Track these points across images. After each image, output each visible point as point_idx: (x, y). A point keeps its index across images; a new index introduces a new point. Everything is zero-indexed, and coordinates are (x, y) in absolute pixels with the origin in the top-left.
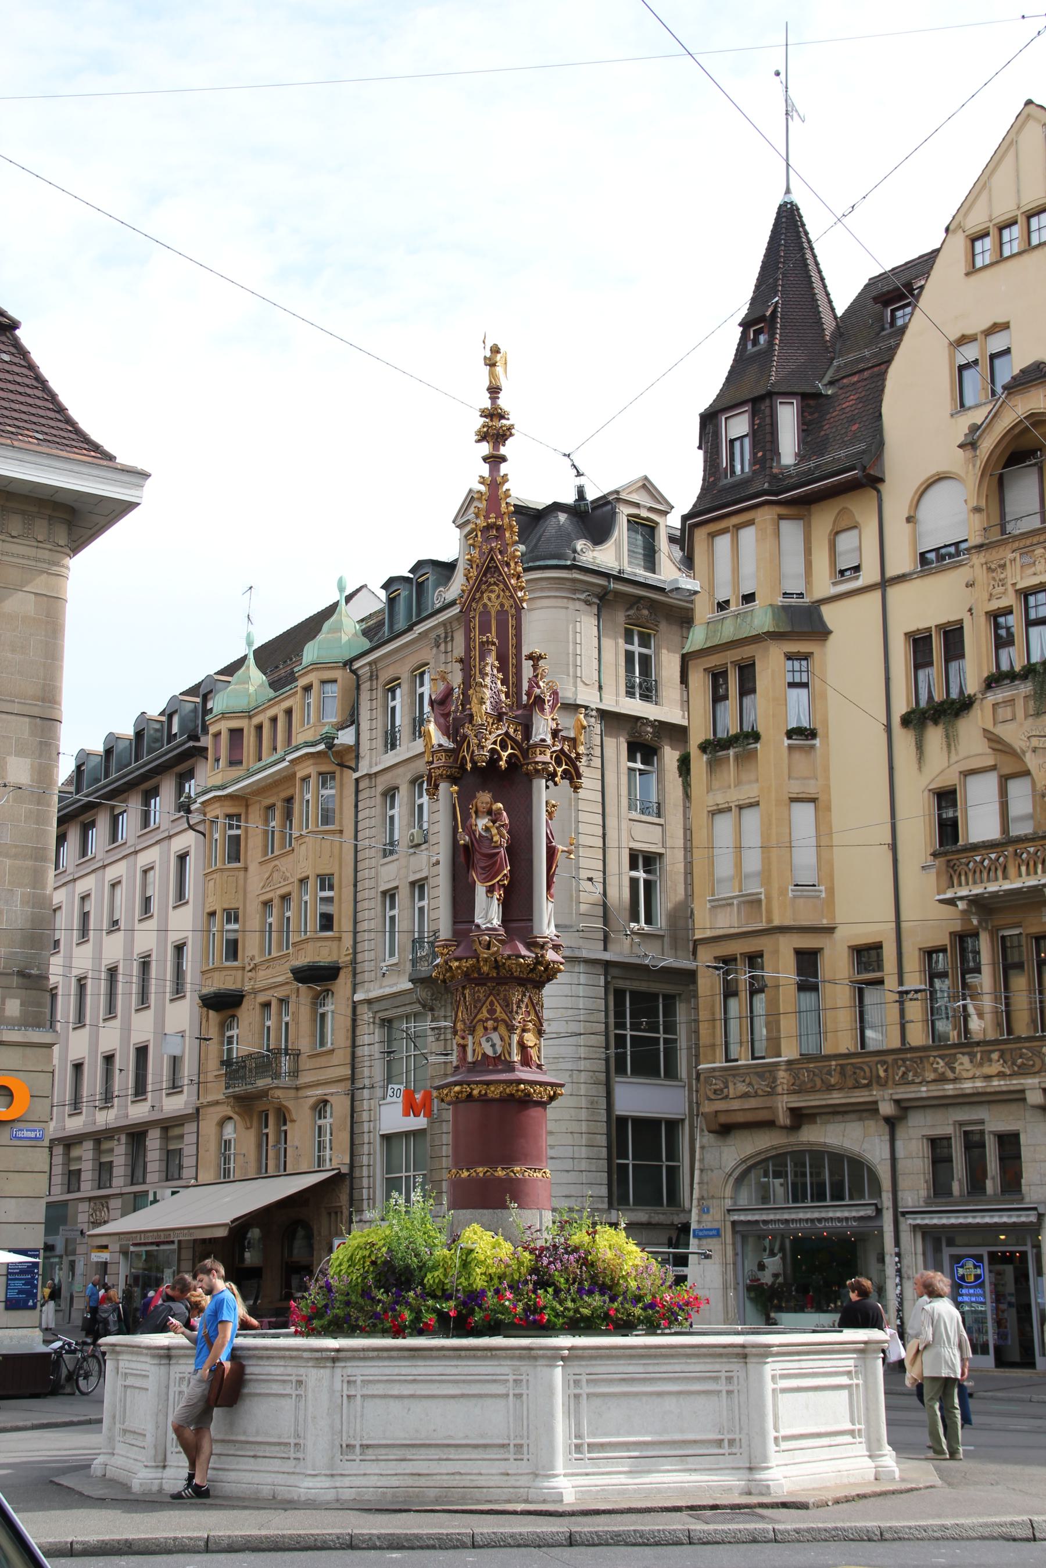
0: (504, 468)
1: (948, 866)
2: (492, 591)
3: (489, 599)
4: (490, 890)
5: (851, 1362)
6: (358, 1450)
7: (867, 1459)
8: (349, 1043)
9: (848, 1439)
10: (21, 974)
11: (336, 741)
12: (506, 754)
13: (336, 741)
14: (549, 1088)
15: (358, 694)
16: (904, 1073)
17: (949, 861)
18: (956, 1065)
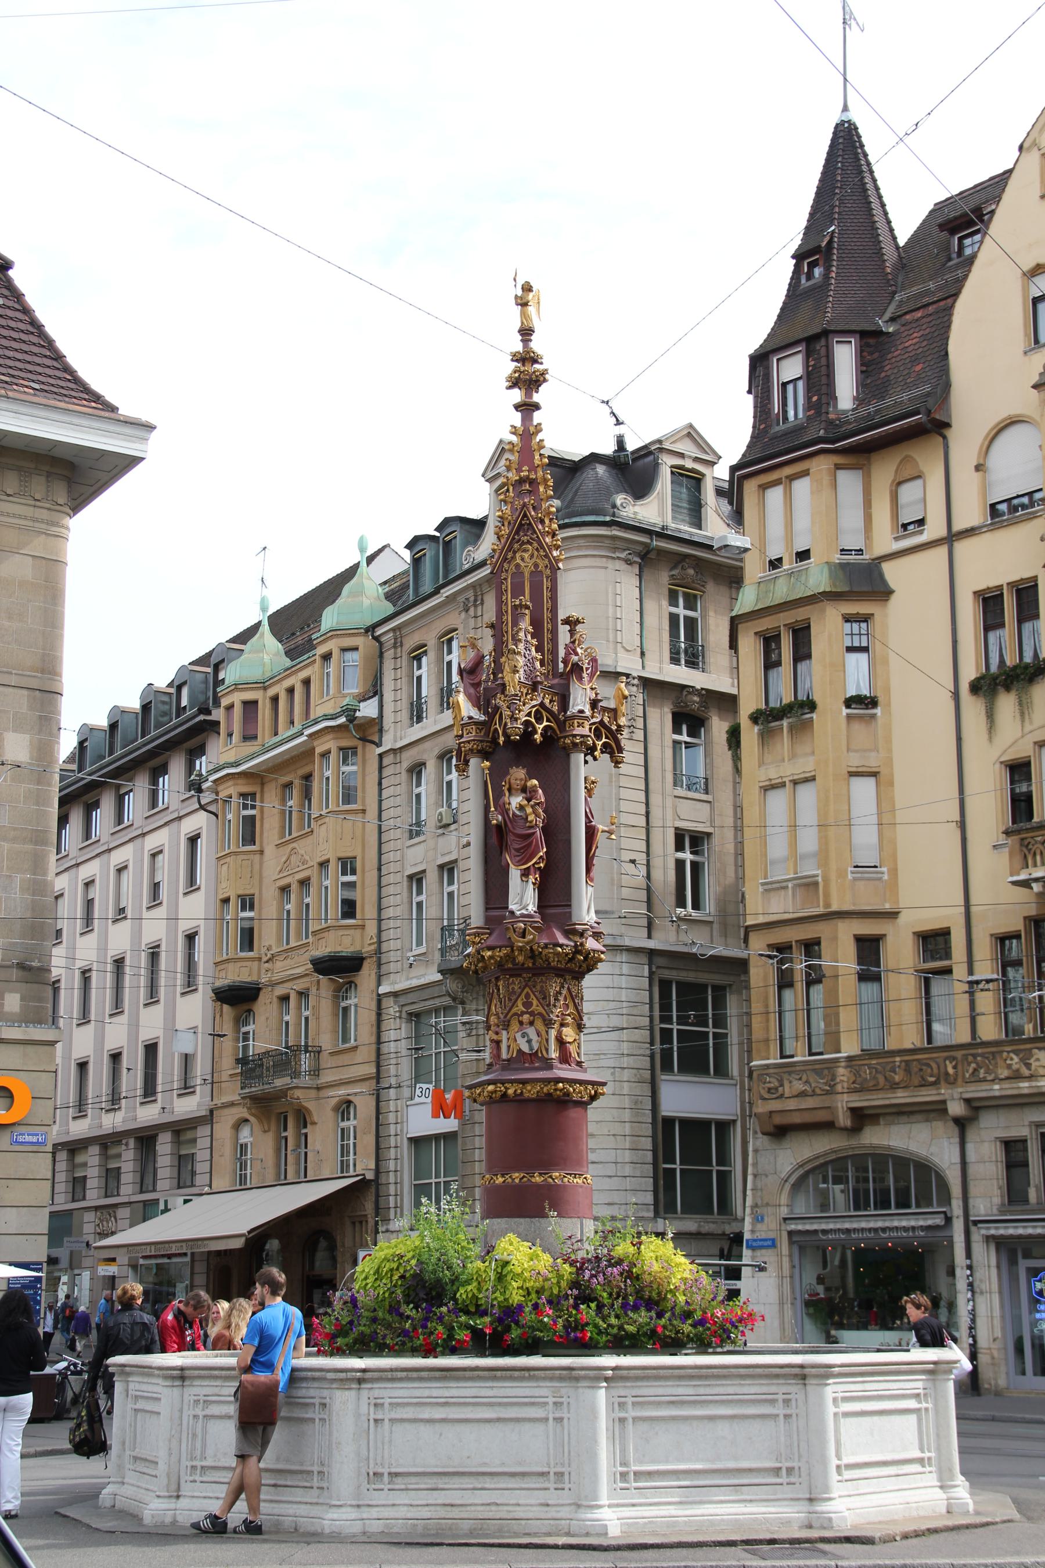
0: (537, 417)
1: (1021, 845)
2: (525, 551)
3: (523, 559)
4: (525, 874)
5: (920, 1384)
6: (386, 1478)
7: (938, 1490)
8: (373, 1039)
9: (916, 1468)
10: (22, 966)
11: (358, 714)
12: (542, 726)
13: (358, 714)
14: (590, 1087)
15: (381, 663)
16: (975, 1070)
17: (1022, 839)
18: (1032, 1061)
